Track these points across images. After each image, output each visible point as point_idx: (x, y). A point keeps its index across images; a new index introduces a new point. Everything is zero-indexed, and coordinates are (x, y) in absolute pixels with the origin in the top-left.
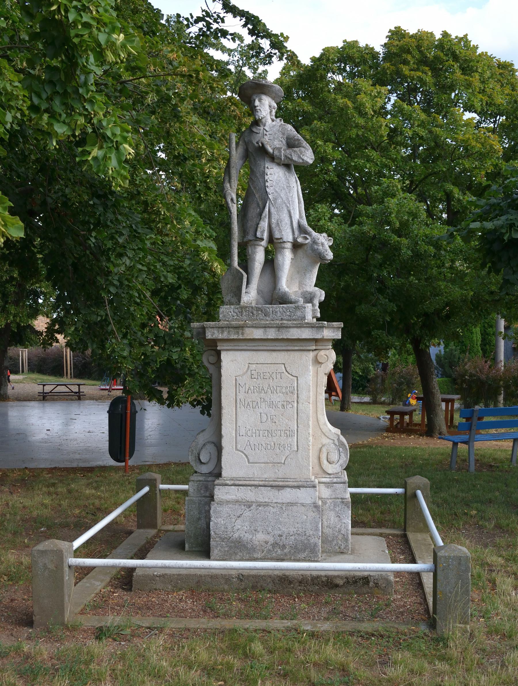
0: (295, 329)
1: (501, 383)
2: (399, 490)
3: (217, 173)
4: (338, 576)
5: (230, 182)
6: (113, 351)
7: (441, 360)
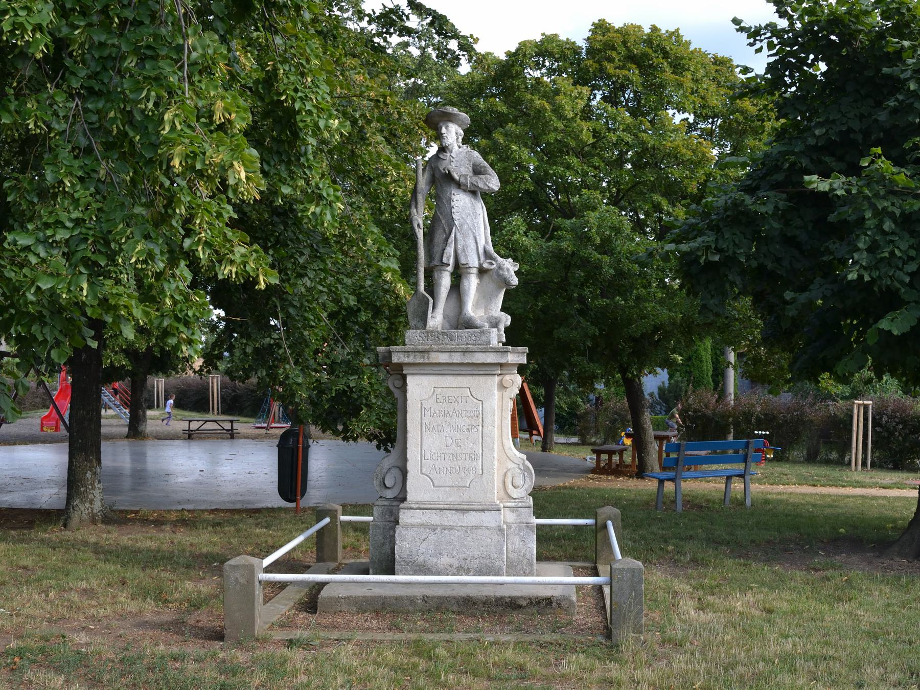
0: (480, 354)
1: (731, 419)
2: (590, 521)
3: (402, 192)
4: (522, 597)
5: (416, 207)
6: (287, 377)
7: (664, 394)
